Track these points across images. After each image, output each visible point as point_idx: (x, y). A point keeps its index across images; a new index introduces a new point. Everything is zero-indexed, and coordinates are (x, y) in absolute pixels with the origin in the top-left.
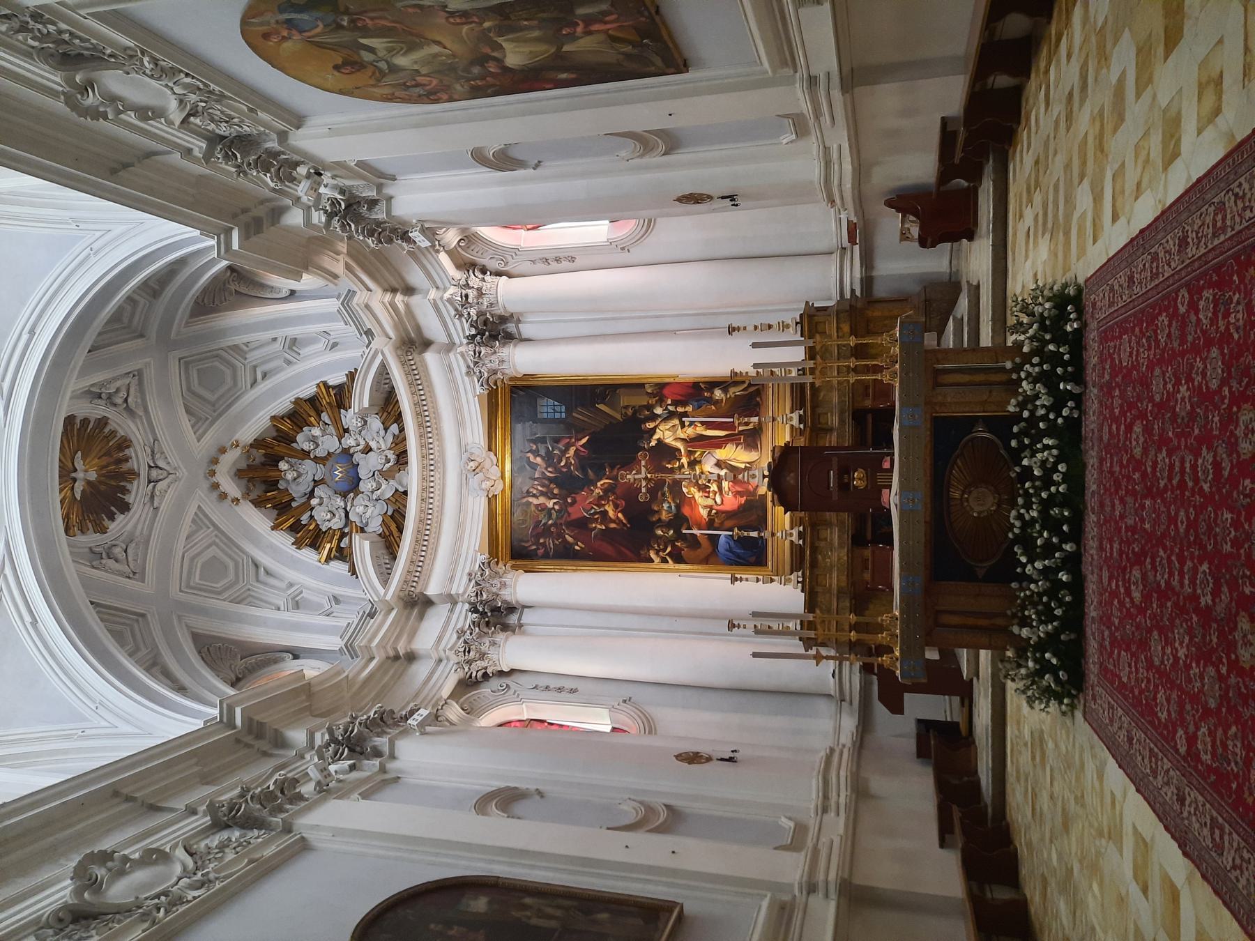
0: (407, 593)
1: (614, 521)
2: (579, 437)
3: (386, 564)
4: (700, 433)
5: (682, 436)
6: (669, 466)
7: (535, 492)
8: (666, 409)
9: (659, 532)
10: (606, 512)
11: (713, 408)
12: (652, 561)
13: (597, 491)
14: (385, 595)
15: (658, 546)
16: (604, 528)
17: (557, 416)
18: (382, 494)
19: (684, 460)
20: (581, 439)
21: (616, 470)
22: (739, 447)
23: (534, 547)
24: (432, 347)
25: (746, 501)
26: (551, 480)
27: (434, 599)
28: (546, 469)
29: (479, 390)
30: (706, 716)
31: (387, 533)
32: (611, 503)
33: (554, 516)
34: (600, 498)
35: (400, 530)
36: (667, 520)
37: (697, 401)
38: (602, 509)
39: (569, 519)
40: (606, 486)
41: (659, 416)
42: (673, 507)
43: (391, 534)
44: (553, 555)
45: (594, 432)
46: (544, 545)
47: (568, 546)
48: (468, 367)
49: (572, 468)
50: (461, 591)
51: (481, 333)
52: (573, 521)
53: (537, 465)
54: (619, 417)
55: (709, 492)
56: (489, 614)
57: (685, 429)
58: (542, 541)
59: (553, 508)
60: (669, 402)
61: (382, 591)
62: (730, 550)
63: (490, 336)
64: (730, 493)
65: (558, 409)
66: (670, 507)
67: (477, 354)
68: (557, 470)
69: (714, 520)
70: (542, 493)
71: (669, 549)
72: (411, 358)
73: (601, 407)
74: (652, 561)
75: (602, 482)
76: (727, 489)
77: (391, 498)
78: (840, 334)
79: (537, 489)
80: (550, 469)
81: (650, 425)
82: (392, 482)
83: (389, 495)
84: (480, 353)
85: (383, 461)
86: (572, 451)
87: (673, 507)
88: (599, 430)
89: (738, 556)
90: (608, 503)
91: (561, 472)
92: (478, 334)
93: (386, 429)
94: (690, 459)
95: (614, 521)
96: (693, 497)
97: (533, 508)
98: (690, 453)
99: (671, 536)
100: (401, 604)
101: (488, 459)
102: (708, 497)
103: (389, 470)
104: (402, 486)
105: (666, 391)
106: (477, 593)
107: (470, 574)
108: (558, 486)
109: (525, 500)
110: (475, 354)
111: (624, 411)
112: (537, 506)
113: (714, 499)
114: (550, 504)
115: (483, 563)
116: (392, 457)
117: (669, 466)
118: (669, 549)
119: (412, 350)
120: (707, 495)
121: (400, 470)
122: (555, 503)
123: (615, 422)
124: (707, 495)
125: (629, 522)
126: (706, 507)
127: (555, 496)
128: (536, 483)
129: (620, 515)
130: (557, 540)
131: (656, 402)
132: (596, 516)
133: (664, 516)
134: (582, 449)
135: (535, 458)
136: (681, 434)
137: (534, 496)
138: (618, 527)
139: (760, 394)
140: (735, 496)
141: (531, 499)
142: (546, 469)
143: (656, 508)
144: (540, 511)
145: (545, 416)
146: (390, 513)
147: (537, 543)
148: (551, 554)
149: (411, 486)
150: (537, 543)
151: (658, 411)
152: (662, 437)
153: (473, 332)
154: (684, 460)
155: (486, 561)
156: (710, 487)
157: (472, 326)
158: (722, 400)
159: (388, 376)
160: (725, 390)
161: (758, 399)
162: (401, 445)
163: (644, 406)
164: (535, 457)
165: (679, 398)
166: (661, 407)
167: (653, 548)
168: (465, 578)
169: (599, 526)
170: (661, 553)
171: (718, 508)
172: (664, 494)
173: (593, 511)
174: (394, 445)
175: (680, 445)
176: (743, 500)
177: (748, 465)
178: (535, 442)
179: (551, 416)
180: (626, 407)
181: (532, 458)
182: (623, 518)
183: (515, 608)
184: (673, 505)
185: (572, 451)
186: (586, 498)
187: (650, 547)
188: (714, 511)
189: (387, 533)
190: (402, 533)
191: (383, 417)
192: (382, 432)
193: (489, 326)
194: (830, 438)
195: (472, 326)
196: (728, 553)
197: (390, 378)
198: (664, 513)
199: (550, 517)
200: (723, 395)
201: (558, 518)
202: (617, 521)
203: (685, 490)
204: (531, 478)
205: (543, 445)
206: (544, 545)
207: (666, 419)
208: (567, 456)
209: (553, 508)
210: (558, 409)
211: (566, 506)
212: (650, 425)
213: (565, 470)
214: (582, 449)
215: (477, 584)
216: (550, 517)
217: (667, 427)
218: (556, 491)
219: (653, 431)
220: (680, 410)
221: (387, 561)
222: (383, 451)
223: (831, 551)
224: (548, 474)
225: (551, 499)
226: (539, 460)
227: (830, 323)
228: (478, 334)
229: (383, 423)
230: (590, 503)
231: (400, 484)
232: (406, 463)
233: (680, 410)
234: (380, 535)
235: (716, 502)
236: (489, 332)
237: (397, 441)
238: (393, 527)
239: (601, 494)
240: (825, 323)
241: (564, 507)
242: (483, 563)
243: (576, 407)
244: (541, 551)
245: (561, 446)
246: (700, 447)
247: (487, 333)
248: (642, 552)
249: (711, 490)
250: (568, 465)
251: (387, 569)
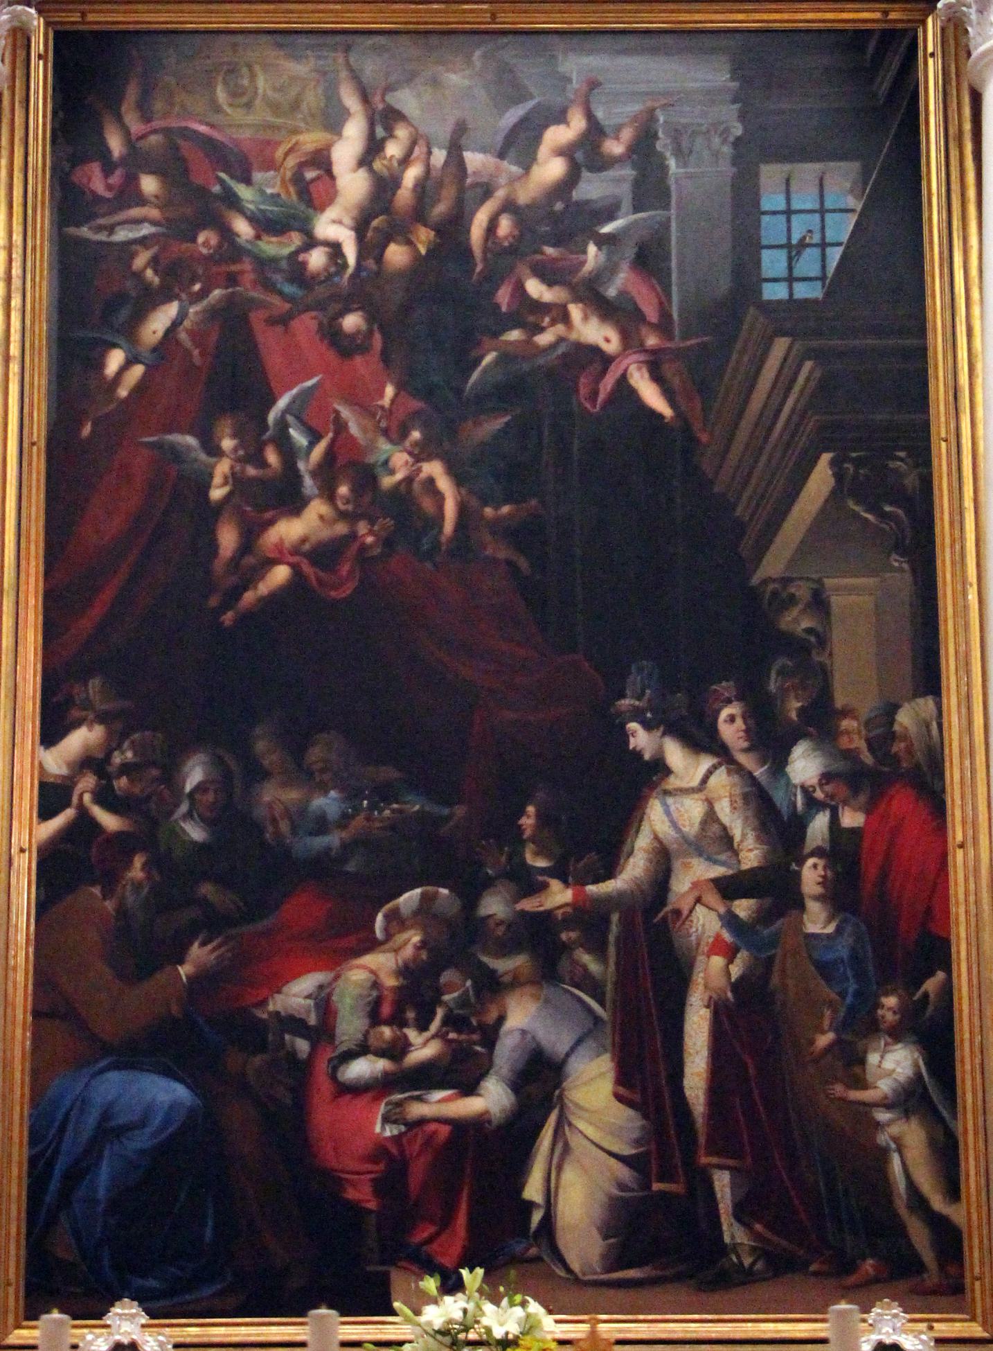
9: (195, 774)
10: (293, 504)
58: (149, 184)
59: (311, 242)
70: (384, 187)
112: (322, 160)
129: (280, 574)
203: (409, 899)
218: (396, 254)
220: (811, 875)
226: (551, 169)
233: (811, 875)
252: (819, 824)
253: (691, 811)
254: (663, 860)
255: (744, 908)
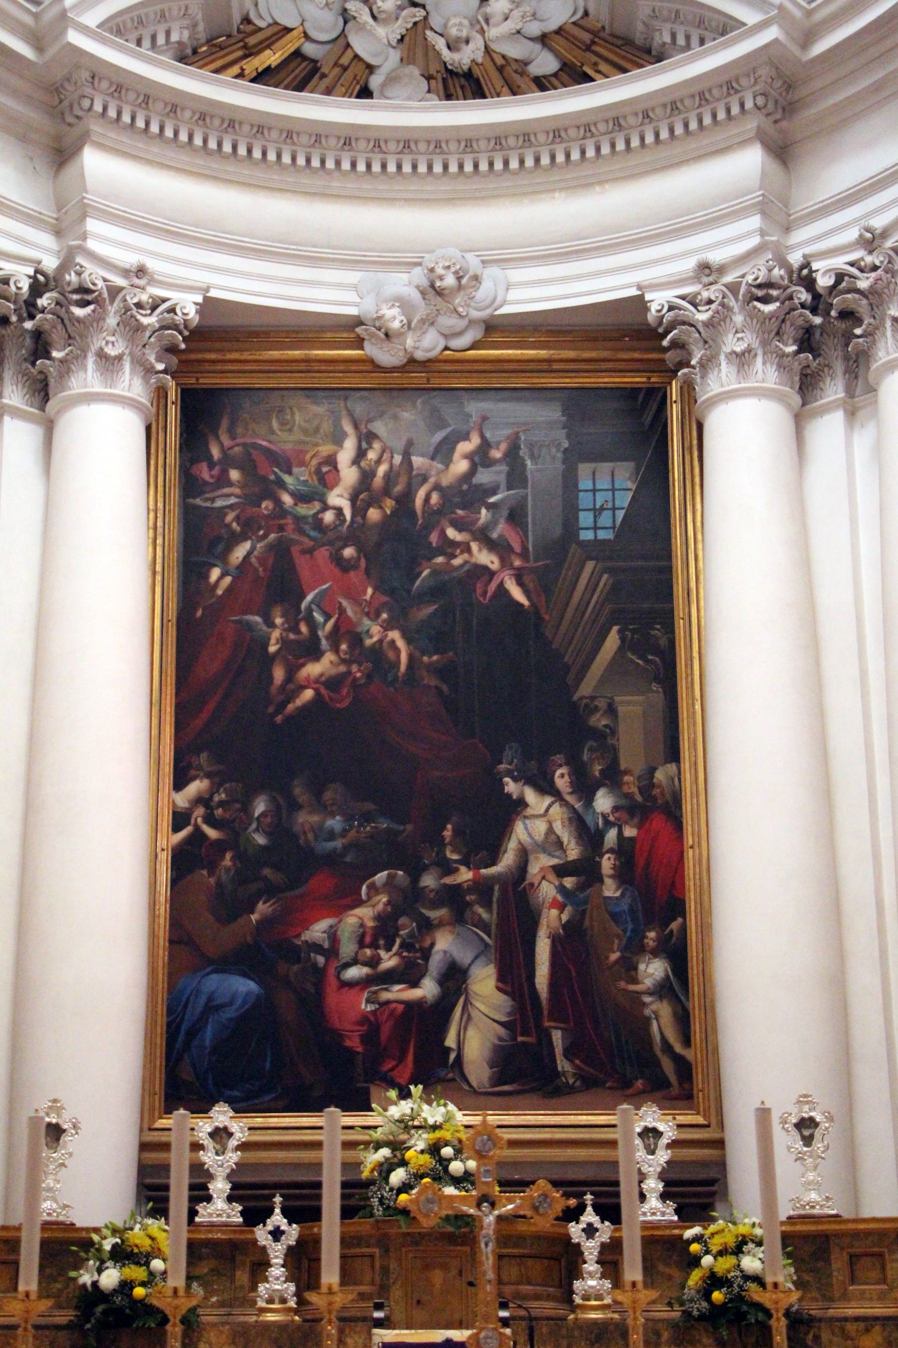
0: (88, 91)
1: (290, 676)
2: (527, 579)
3: (168, 33)
4: (544, 921)
5: (534, 869)
6: (448, 833)
7: (372, 455)
8: (608, 824)
9: (260, 807)
10: (315, 654)
11: (614, 956)
12: (179, 784)
13: (376, 630)
14: (85, 30)
15: (221, 804)
16: (273, 649)
17: (586, 518)
18: (362, 28)
19: (465, 875)
20: (520, 583)
21: (434, 682)
22: (501, 1031)
23: (216, 452)
24: (774, 167)
25: (350, 1051)
26: (406, 499)
27: (70, 171)
28: (437, 487)
29: (658, 300)
30: (32, 115)
31: (252, 41)
32: (343, 668)
33: (304, 510)
34: (356, 640)
35: (263, 77)
36: (297, 828)
37: (632, 910)
38: (324, 643)
39: (295, 550)
40: (391, 655)
41: (589, 800)
42: (331, 845)
43: (250, 52)
44: (196, 507)
45: (540, 618)
46: (223, 480)
47: (220, 547)
48: (722, 270)
49: (440, 560)
50: (92, 244)
51: (818, 303)
52: (291, 559)
53: (447, 461)
54: (586, 689)
55: (374, 945)
56: (28, 325)
57: (551, 876)
58: (234, 475)
59: (326, 507)
60: (630, 832)
61: (93, 18)
62: (212, 1007)
63: (809, 330)
64: (370, 1008)
65: (605, 519)
66: (331, 835)
67: (760, 293)
68: (434, 516)
69: (298, 961)
70: (367, 476)
71: (212, 833)
72: (749, 105)
73: (612, 641)
74: (179, 784)
75: (401, 644)
76: (385, 996)
77: (348, 55)
78: (850, 1327)
79: (379, 462)
80: (435, 498)
81: (562, 779)
82: (394, 56)
83: (360, 45)
84: (765, 300)
85: (454, 32)
86: (485, 558)
87: (331, 845)
88: (548, 633)
89: (193, 1033)
90: (343, 661)
91: (428, 528)
92: (816, 296)
93: (543, 39)
94: (470, 890)
95: (290, 676)
96: (359, 903)
97: (325, 449)
98: (482, 888)
99: (250, 840)
100: (58, 74)
101: (463, 323)
102: (362, 944)
103: (429, 49)
104: (384, 85)
105: (658, 822)
106: (88, 291)
107: (141, 271)
108: (387, 520)
109: (348, 428)
110: (759, 286)
111: (602, 704)
112: (331, 461)
113: (354, 962)
114: (338, 498)
115: (172, 310)
116: (463, 58)
117: (448, 833)
118: (212, 833)
119: (771, 105)
120: (368, 939)
121: (429, 78)
122: (339, 511)
123: (570, 678)
124: (368, 939)
125: (289, 719)
126: (333, 936)
127: (359, 510)
128: (398, 459)
129: (308, 694)
130: (237, 518)
131: (629, 796)
132: (304, 628)
133: (305, 819)
134: (493, 587)
135: (466, 456)
136: (540, 864)
137: (361, 454)
138: (273, 690)
139: (652, 1090)
140: (365, 1019)
141: (349, 446)
142: (437, 487)
143: (328, 795)
144: (318, 472)
145: (585, 483)
146: (309, 49)
147: (227, 461)
148: (198, 501)
149: (386, 108)
150: (227, 461)
151: (603, 802)
152: (529, 811)
153: (824, 282)
154: (465, 875)
155: (179, 318)
156: (388, 949)
157: (840, 277)
158: (635, 981)
159: (695, 41)
160: (663, 990)
161: (639, 1084)
162: (498, 82)
163: (615, 762)
164: (469, 456)
165: (641, 862)
166: (616, 809)
167: (214, 789)
168: (130, 259)
169: (276, 634)
170: (200, 811)
171: (332, 971)
172: (367, 818)
173: (318, 617)
174: (500, 61)
175: (508, 860)
176: (354, 1043)
177: (453, 1056)
178: (513, 455)
179: (585, 500)
180: (611, 710)
181: (465, 447)
182: (299, 702)
183: (46, 398)
184: (338, 844)
185: (485, 558)
186: (355, 599)
187: (218, 780)
188: (321, 960)
189: (252, 41)
190: (253, 80)
191: (576, 31)
192: (535, 29)
193: (841, 325)
194: (549, 1298)
195: (840, 277)
196: (202, 1000)
197: (688, 47)
198: (315, 819)
199: (301, 498)
200: (648, 983)
201: (299, 520)
202: (292, 688)
203: (381, 877)
204: (410, 443)
205: (502, 479)
206: (223, 480)
207: (578, 822)
208: (474, 546)
209: (326, 507)
210: (605, 519)
211: (330, 543)
212: (562, 779)
213: (434, 538)
214: (493, 587)
215: (114, 292)
216: (301, 498)
217: (558, 827)
218: (374, 514)
219: (546, 787)
220: (607, 864)
221: (175, 37)
222: (482, 32)
223: (221, 1304)
224: (421, 494)
225: (353, 499)
226: (460, 466)
227: (882, 1297)
228: (816, 296)
229: (559, 31)
230: (342, 611)
231: (392, 79)
232: (449, 97)
233: (607, 864)
234: (247, 20)
235: (347, 965)
236: (821, 326)
237: (508, 69)
238: (271, 58)
239: (368, 642)
240: (884, 1281)
241: (331, 535)
242: (172, 310)
243: (610, 571)
244: (205, 473)
245: (500, 530)
246: (503, 920)
247: (818, 320)
248: (204, 756)
249: (382, 953)
250: (449, 548)
251: (154, 38)
252: (611, 836)
253: (540, 828)
254: (524, 856)
255: (569, 882)
